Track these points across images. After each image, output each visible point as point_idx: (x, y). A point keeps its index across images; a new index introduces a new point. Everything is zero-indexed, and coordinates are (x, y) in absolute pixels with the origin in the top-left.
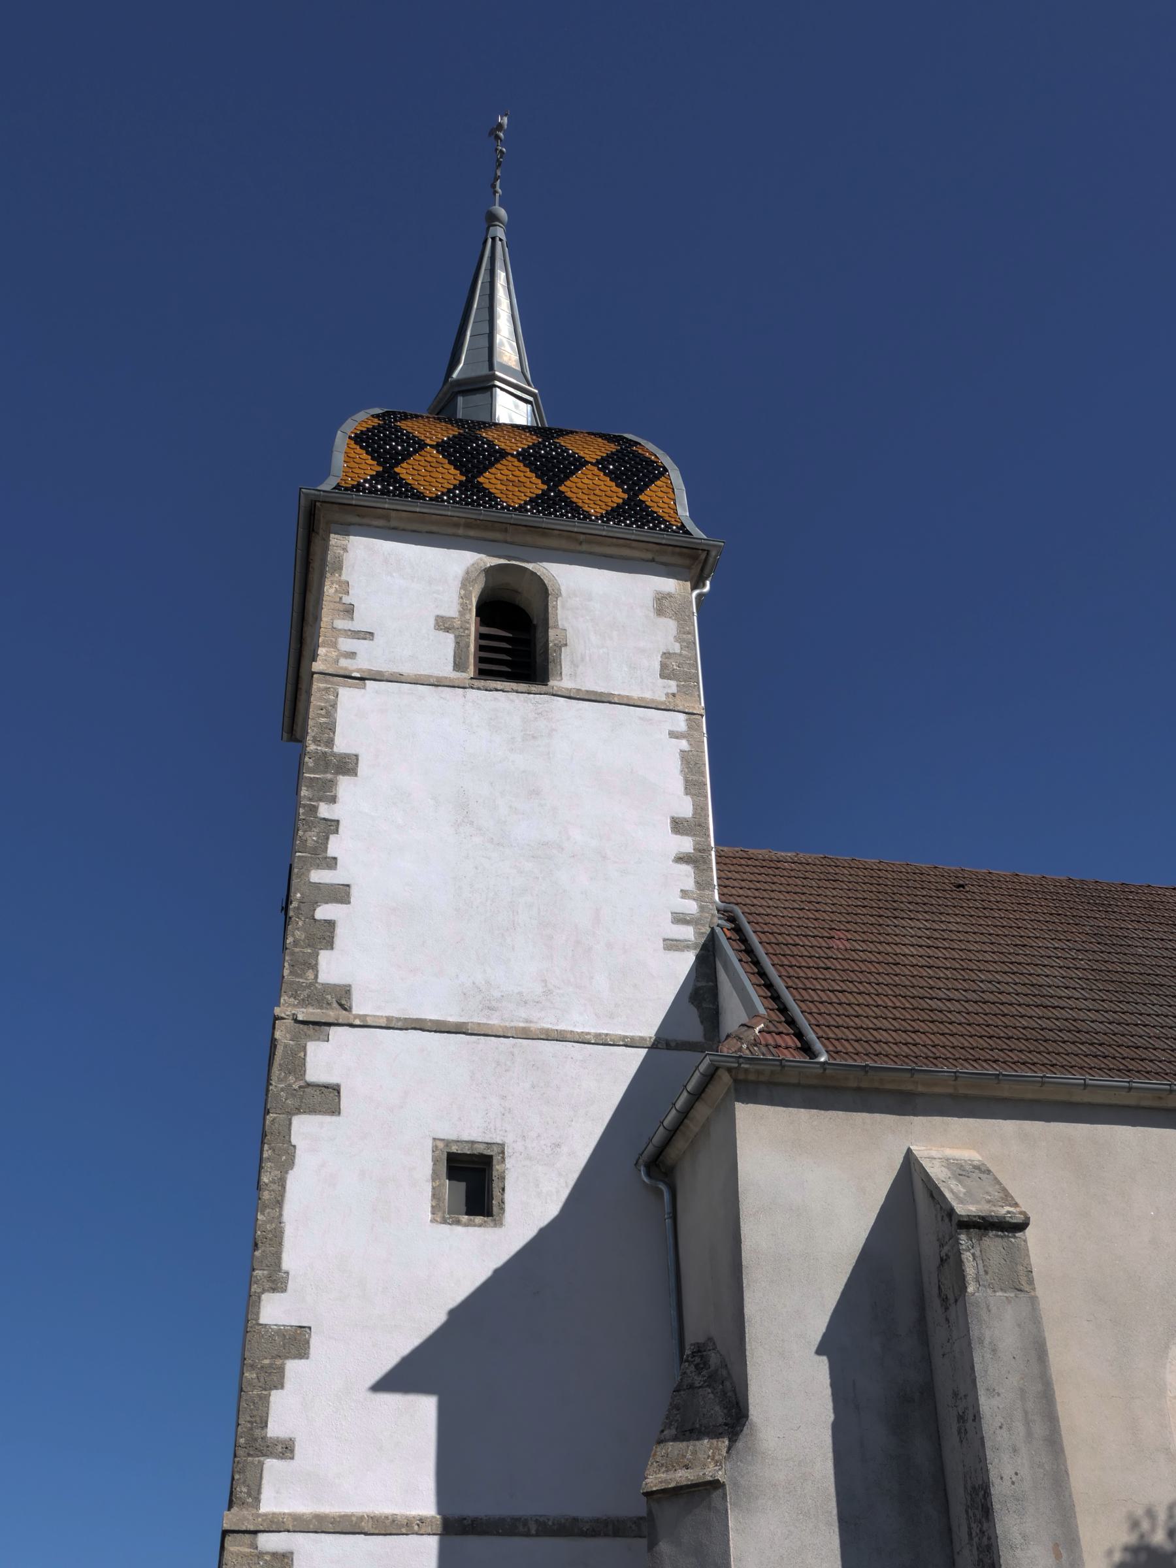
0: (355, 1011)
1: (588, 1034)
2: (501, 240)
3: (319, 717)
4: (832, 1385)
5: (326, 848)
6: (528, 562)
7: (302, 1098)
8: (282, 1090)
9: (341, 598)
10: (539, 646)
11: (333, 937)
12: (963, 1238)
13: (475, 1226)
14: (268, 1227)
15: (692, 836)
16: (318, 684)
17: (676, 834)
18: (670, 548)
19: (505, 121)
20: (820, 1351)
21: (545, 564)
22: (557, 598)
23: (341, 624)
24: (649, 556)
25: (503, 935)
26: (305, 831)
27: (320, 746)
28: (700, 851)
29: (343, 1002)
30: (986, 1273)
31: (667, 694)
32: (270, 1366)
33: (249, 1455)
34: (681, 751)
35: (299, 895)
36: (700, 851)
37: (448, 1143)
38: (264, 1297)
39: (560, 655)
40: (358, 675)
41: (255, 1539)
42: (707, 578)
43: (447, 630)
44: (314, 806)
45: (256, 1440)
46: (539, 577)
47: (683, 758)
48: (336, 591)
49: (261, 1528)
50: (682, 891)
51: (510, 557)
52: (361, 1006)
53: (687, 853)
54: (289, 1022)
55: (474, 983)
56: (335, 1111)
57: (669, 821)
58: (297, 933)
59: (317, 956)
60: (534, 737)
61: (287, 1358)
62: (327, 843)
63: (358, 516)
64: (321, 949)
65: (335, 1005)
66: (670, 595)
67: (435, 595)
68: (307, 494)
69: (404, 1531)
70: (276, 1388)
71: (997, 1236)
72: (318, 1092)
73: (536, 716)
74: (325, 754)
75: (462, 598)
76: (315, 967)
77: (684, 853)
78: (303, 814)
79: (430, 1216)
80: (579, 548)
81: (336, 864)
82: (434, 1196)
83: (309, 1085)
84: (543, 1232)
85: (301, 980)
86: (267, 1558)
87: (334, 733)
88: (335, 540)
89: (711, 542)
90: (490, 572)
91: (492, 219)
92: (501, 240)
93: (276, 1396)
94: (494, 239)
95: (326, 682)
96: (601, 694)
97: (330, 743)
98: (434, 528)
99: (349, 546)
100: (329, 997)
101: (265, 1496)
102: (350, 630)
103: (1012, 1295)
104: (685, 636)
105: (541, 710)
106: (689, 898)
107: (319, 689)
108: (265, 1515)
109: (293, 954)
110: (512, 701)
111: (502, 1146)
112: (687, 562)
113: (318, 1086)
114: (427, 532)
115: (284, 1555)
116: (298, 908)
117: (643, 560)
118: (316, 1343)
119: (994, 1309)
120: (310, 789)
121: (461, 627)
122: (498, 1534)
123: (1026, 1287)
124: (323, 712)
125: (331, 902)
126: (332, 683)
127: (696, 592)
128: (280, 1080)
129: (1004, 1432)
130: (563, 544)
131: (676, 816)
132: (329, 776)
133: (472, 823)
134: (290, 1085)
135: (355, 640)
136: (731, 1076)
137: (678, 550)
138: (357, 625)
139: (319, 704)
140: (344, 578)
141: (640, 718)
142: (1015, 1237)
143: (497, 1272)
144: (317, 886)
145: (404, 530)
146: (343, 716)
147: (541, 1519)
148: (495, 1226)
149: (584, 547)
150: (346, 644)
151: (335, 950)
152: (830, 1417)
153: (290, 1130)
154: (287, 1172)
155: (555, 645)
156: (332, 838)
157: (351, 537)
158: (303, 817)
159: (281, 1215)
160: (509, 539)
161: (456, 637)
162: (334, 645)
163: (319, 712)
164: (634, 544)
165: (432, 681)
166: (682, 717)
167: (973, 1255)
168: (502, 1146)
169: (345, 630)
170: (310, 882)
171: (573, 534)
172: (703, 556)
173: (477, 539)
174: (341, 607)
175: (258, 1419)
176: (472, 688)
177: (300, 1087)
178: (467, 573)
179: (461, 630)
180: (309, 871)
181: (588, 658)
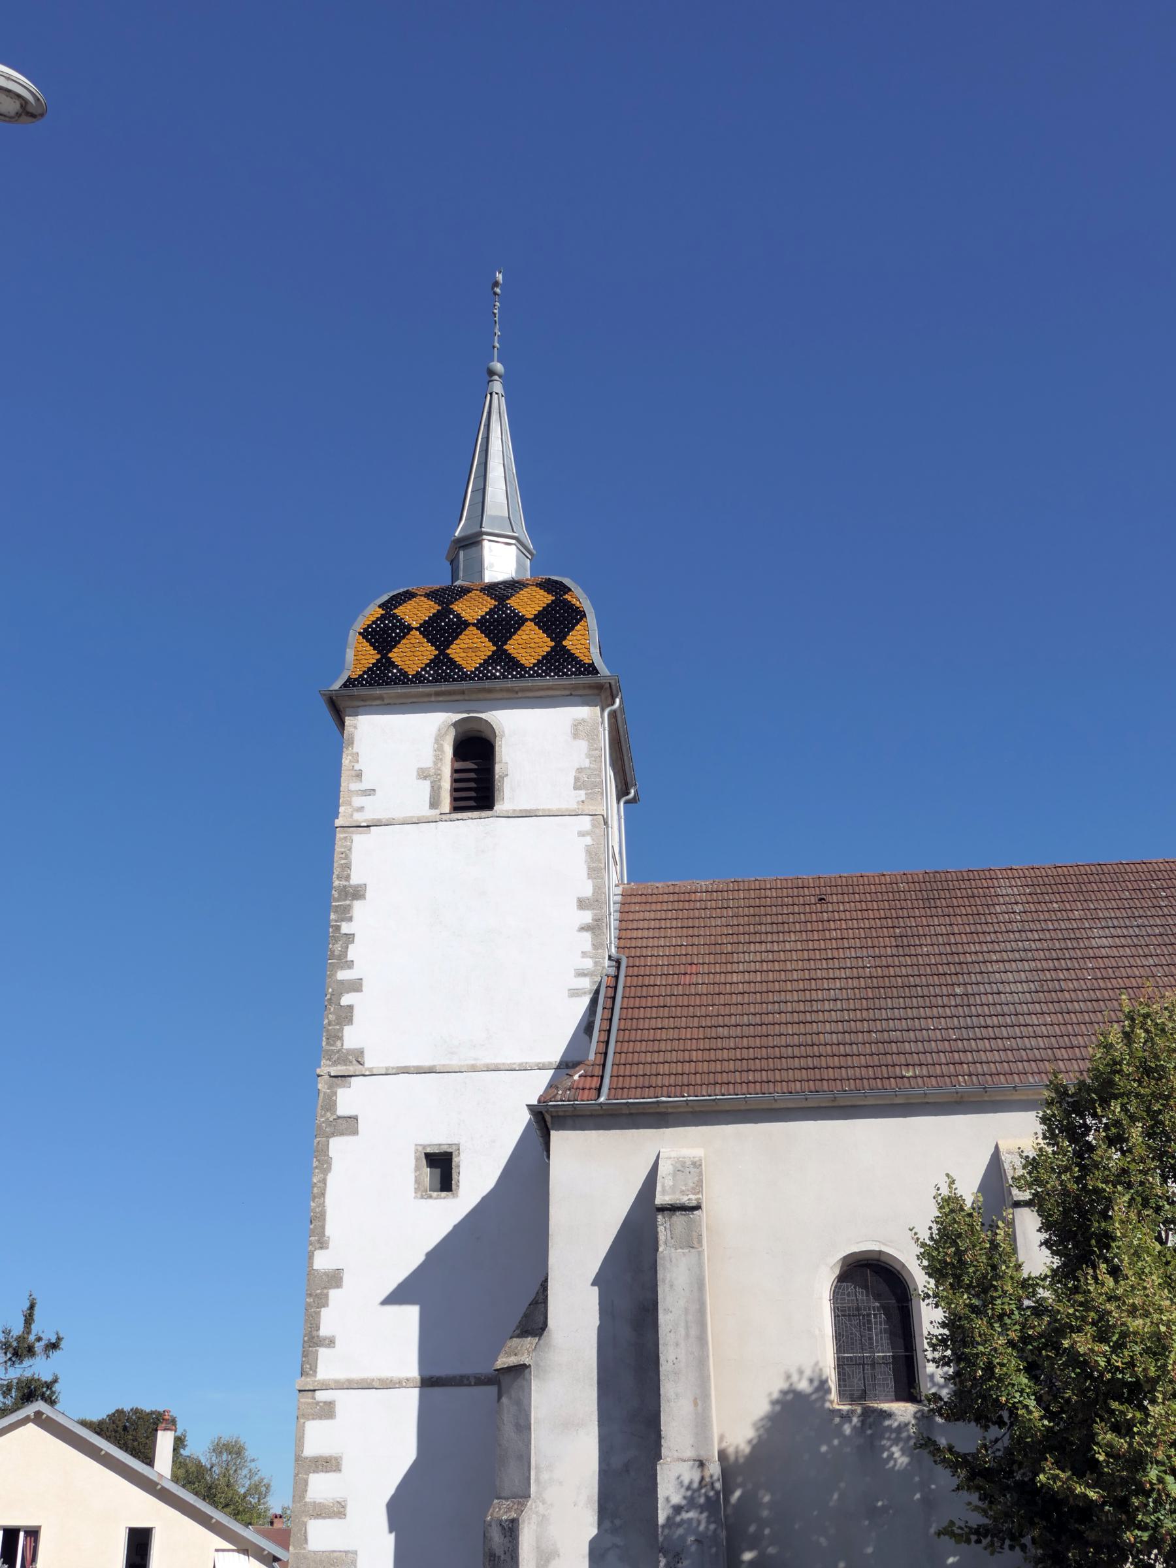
0: (367, 1065)
1: (514, 1064)
4: (599, 1304)
6: (482, 712)
7: (335, 1126)
8: (323, 1122)
12: (660, 1218)
13: (441, 1198)
14: (317, 1210)
16: (340, 835)
20: (593, 1284)
21: (494, 712)
23: (354, 786)
24: (568, 692)
26: (333, 944)
29: (360, 1060)
30: (672, 1238)
31: (578, 802)
32: (321, 1294)
33: (310, 1347)
35: (330, 990)
36: (596, 920)
37: (424, 1147)
38: (315, 1253)
41: (314, 1394)
43: (425, 778)
44: (338, 926)
45: (314, 1338)
48: (350, 761)
49: (317, 1388)
52: (370, 1062)
54: (327, 1077)
56: (355, 1132)
58: (330, 1016)
61: (330, 1288)
63: (362, 700)
65: (355, 1062)
69: (397, 1386)
70: (324, 1307)
71: (682, 1214)
72: (345, 1122)
74: (345, 886)
76: (341, 1038)
79: (413, 1194)
80: (517, 696)
82: (416, 1181)
83: (339, 1117)
84: (484, 1199)
85: (334, 1048)
86: (321, 1404)
90: (456, 725)
91: (491, 373)
93: (324, 1311)
94: (491, 394)
97: (348, 878)
100: (350, 1057)
101: (318, 1370)
103: (687, 1251)
104: (593, 752)
108: (319, 1381)
109: (328, 1031)
111: (458, 1145)
112: (596, 692)
113: (345, 1117)
115: (330, 1403)
116: (330, 999)
118: (347, 1278)
119: (674, 1260)
122: (452, 1385)
123: (696, 1245)
124: (343, 856)
126: (348, 832)
128: (322, 1116)
129: (672, 1335)
132: (348, 902)
134: (328, 1119)
138: (365, 785)
140: (355, 750)
142: (693, 1214)
143: (455, 1227)
144: (342, 982)
145: (395, 704)
146: (356, 858)
147: (478, 1376)
148: (454, 1197)
150: (357, 801)
152: (596, 1322)
153: (328, 1148)
154: (327, 1175)
159: (324, 1202)
160: (467, 698)
161: (431, 783)
162: (349, 803)
167: (665, 1227)
168: (458, 1145)
174: (354, 773)
175: (315, 1326)
177: (334, 1119)
180: (336, 972)
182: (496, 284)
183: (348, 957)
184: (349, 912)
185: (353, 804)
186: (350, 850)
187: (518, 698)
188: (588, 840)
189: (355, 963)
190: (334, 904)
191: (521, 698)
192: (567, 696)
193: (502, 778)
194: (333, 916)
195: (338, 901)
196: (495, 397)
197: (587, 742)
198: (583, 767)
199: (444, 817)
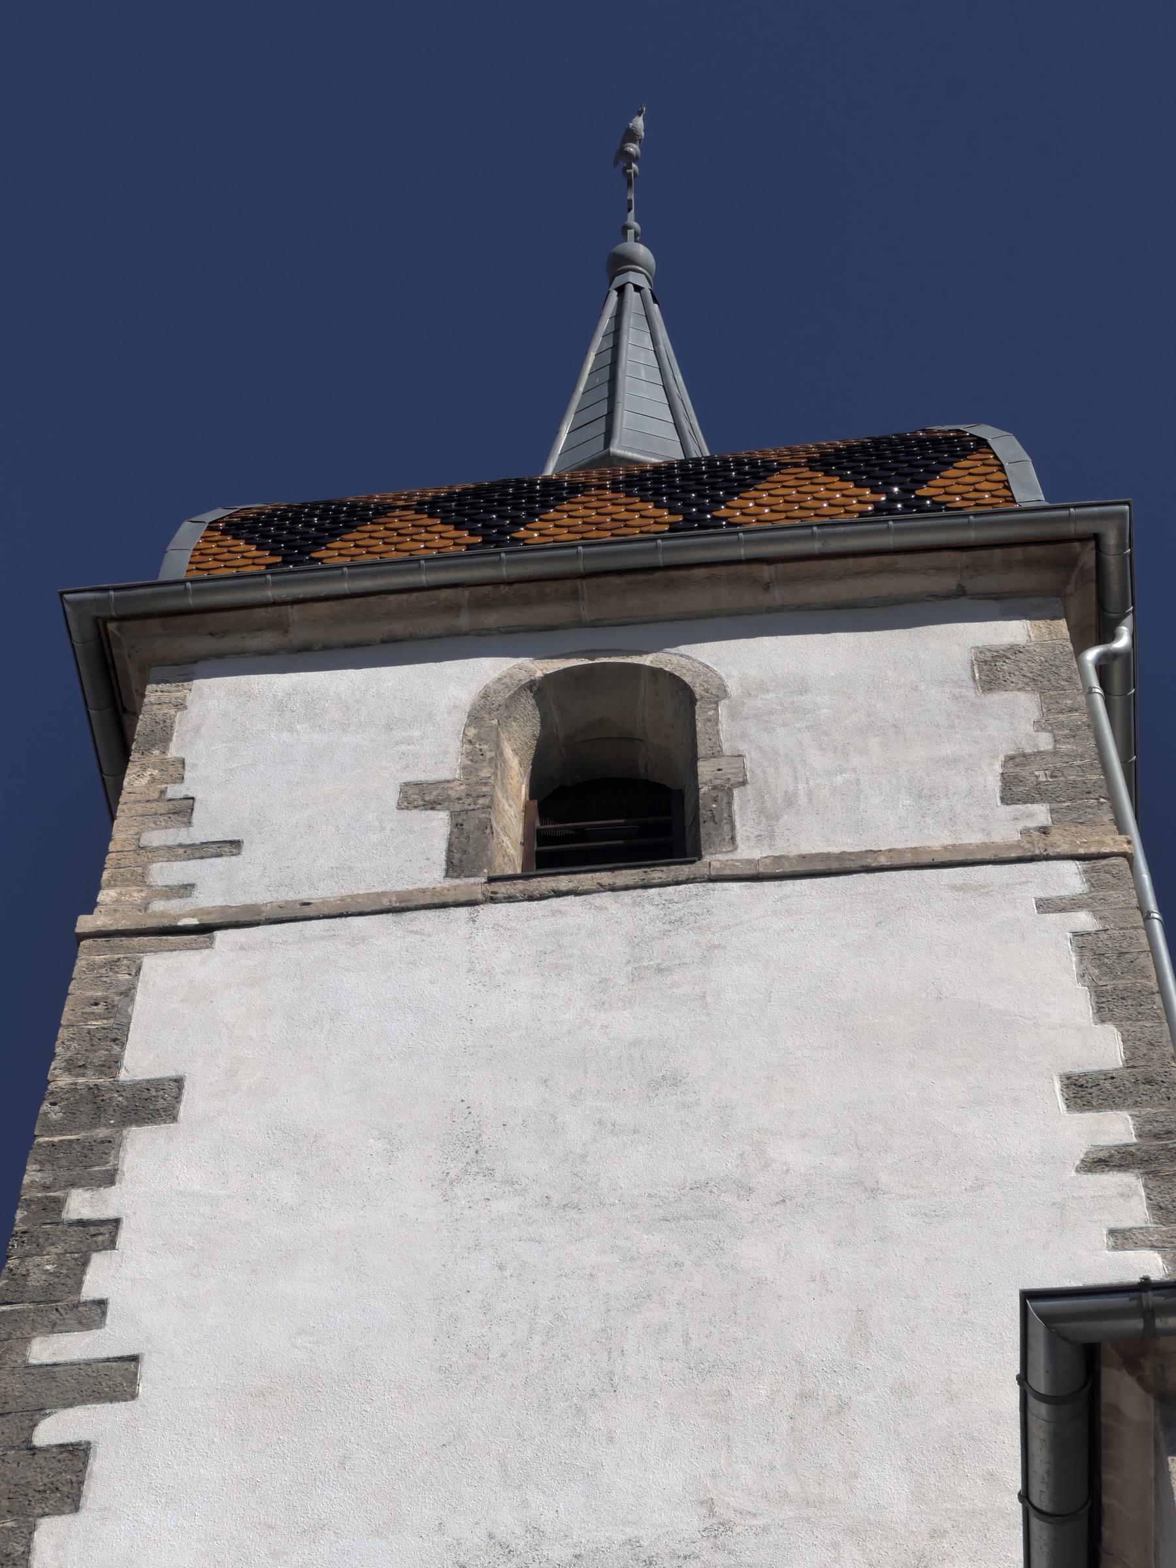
2: (638, 289)
3: (86, 1020)
5: (80, 1283)
6: (640, 653)
9: (163, 792)
10: (688, 809)
11: (81, 1483)
15: (1128, 1107)
16: (88, 957)
17: (1082, 1111)
18: (998, 553)
19: (639, 123)
21: (683, 649)
22: (717, 703)
24: (948, 582)
25: (579, 1410)
26: (22, 1258)
27: (83, 1075)
28: (1157, 1136)
31: (1025, 832)
34: (1075, 934)
36: (1157, 1136)
39: (730, 804)
40: (194, 921)
42: (1118, 622)
46: (671, 675)
47: (1081, 950)
48: (153, 780)
50: (1112, 1232)
51: (593, 651)
53: (1118, 1148)
55: (491, 1536)
57: (1058, 1086)
59: (31, 1533)
60: (660, 970)
62: (83, 1272)
63: (211, 634)
64: (44, 1515)
66: (1015, 650)
67: (403, 748)
68: (78, 604)
73: (667, 927)
74: (95, 1090)
75: (470, 742)
77: (1108, 1148)
78: (23, 1220)
80: (764, 599)
81: (104, 1313)
87: (123, 1045)
88: (154, 693)
89: (1096, 509)
91: (621, 263)
92: (638, 289)
94: (621, 290)
95: (112, 950)
96: (842, 856)
97: (113, 1064)
98: (399, 627)
99: (189, 698)
102: (180, 845)
104: (1062, 717)
105: (678, 915)
106: (1137, 1246)
107: (92, 967)
110: (601, 909)
114: (383, 642)
117: (936, 597)
120: (48, 1166)
121: (468, 795)
125: (83, 1402)
126: (127, 950)
127: (1092, 655)
130: (726, 596)
131: (1077, 1070)
132: (102, 1133)
133: (490, 1172)
135: (193, 862)
136: (1141, 1381)
137: (1018, 553)
138: (201, 830)
139: (89, 993)
140: (173, 752)
141: (954, 888)
144: (49, 1370)
145: (326, 648)
149: (778, 595)
150: (165, 873)
151: (83, 1511)
155: (715, 788)
156: (98, 1261)
157: (196, 682)
158: (24, 1228)
160: (586, 615)
161: (453, 815)
162: (141, 879)
163: (88, 1010)
164: (902, 561)
165: (385, 903)
166: (1072, 867)
169: (169, 848)
170: (28, 1366)
171: (744, 569)
172: (1088, 557)
173: (509, 631)
174: (163, 807)
176: (493, 900)
178: (485, 695)
179: (469, 800)
181: (803, 799)
182: (631, 136)
183: (85, 1289)
184: (103, 1158)
185: (149, 880)
186: (128, 993)
187: (769, 610)
188: (1084, 920)
189: (111, 1310)
190: (41, 1140)
191: (780, 609)
192: (947, 597)
193: (725, 791)
194: (32, 1175)
195: (60, 1128)
196: (632, 296)
197: (1036, 697)
198: (1028, 750)
199: (502, 888)
